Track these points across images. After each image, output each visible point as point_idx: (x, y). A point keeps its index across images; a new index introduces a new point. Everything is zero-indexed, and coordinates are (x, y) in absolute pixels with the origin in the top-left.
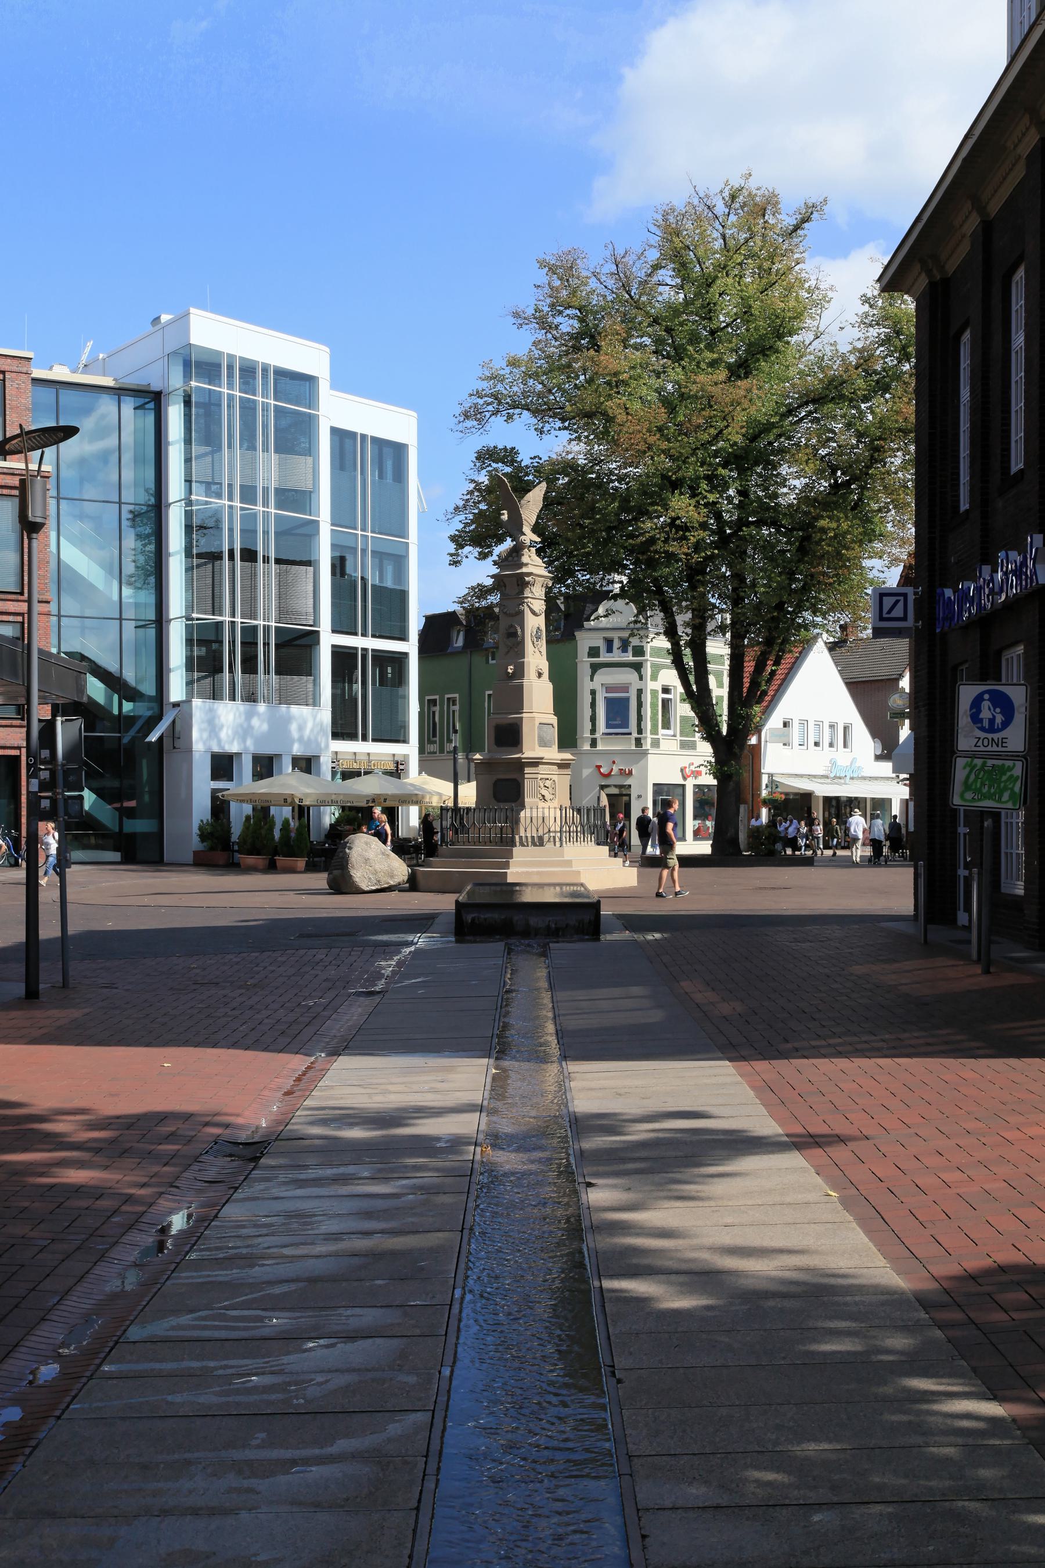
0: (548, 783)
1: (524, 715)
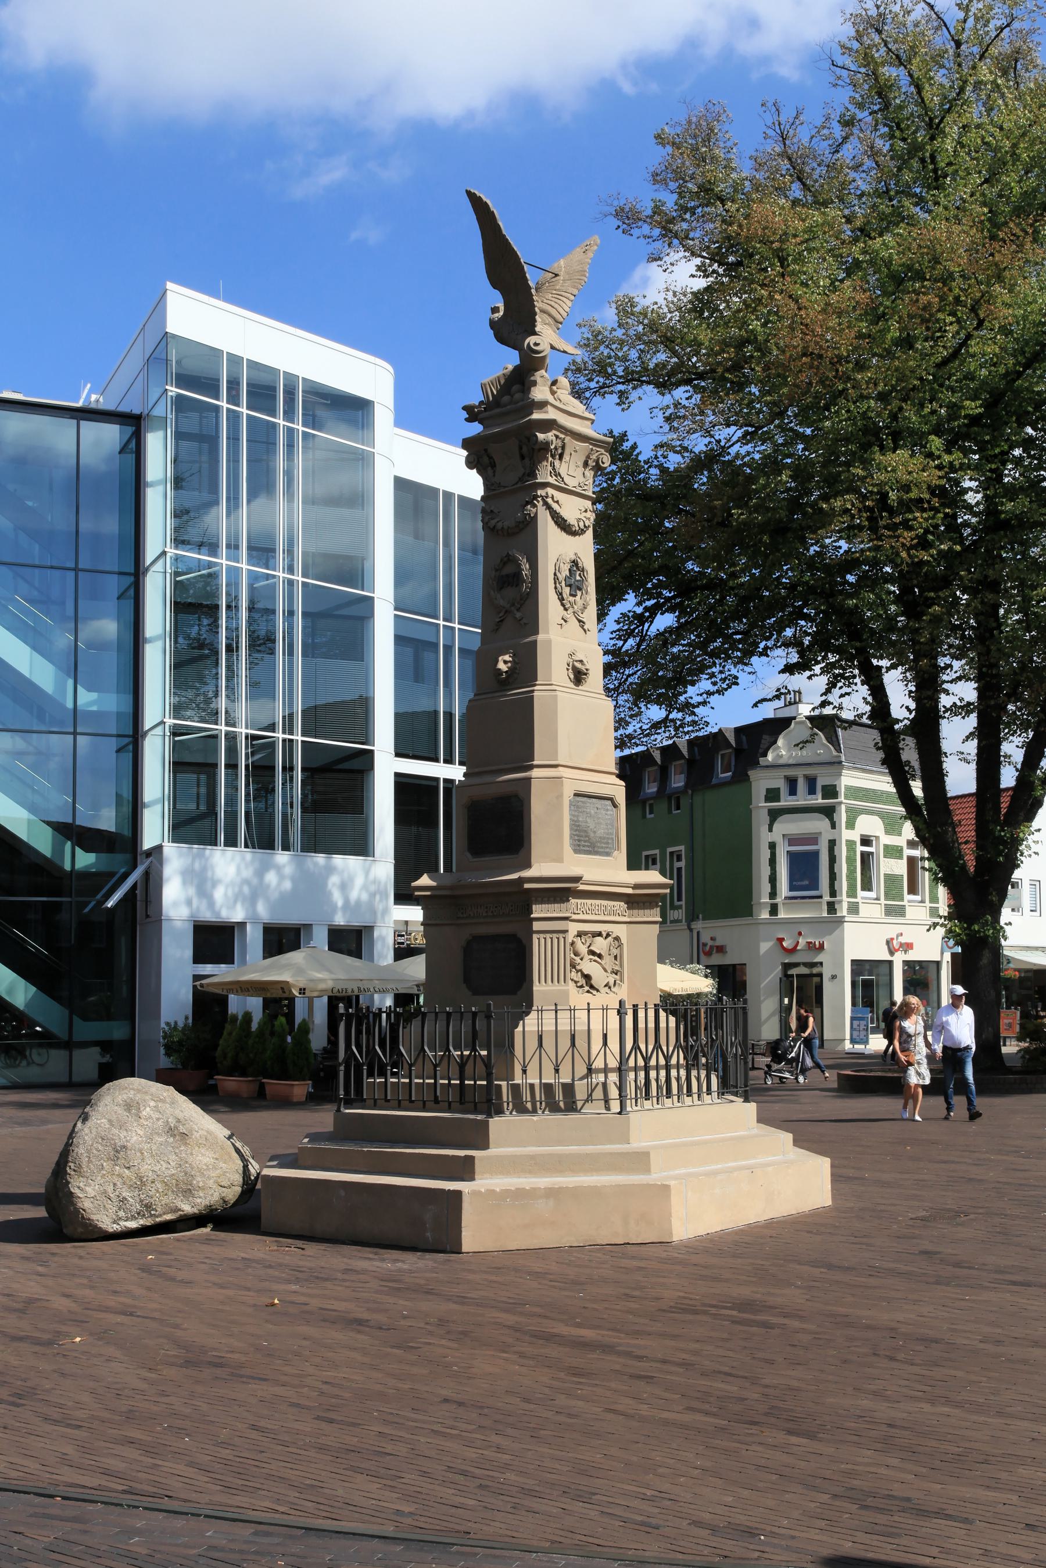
0: (600, 945)
1: (535, 773)
